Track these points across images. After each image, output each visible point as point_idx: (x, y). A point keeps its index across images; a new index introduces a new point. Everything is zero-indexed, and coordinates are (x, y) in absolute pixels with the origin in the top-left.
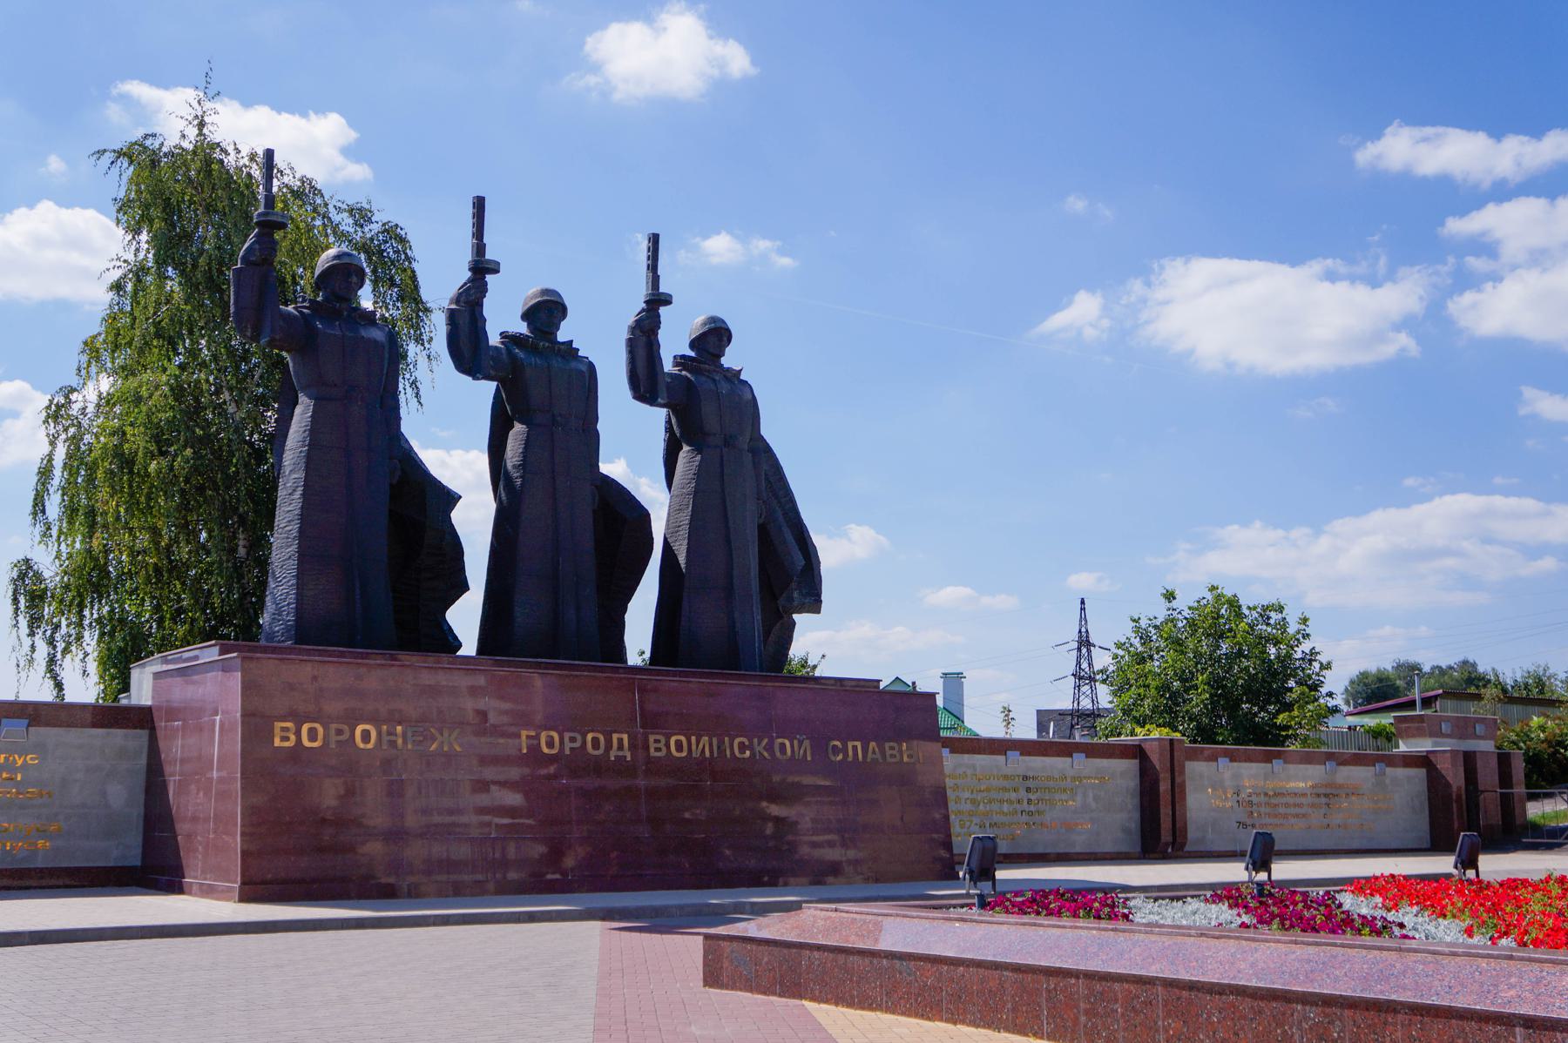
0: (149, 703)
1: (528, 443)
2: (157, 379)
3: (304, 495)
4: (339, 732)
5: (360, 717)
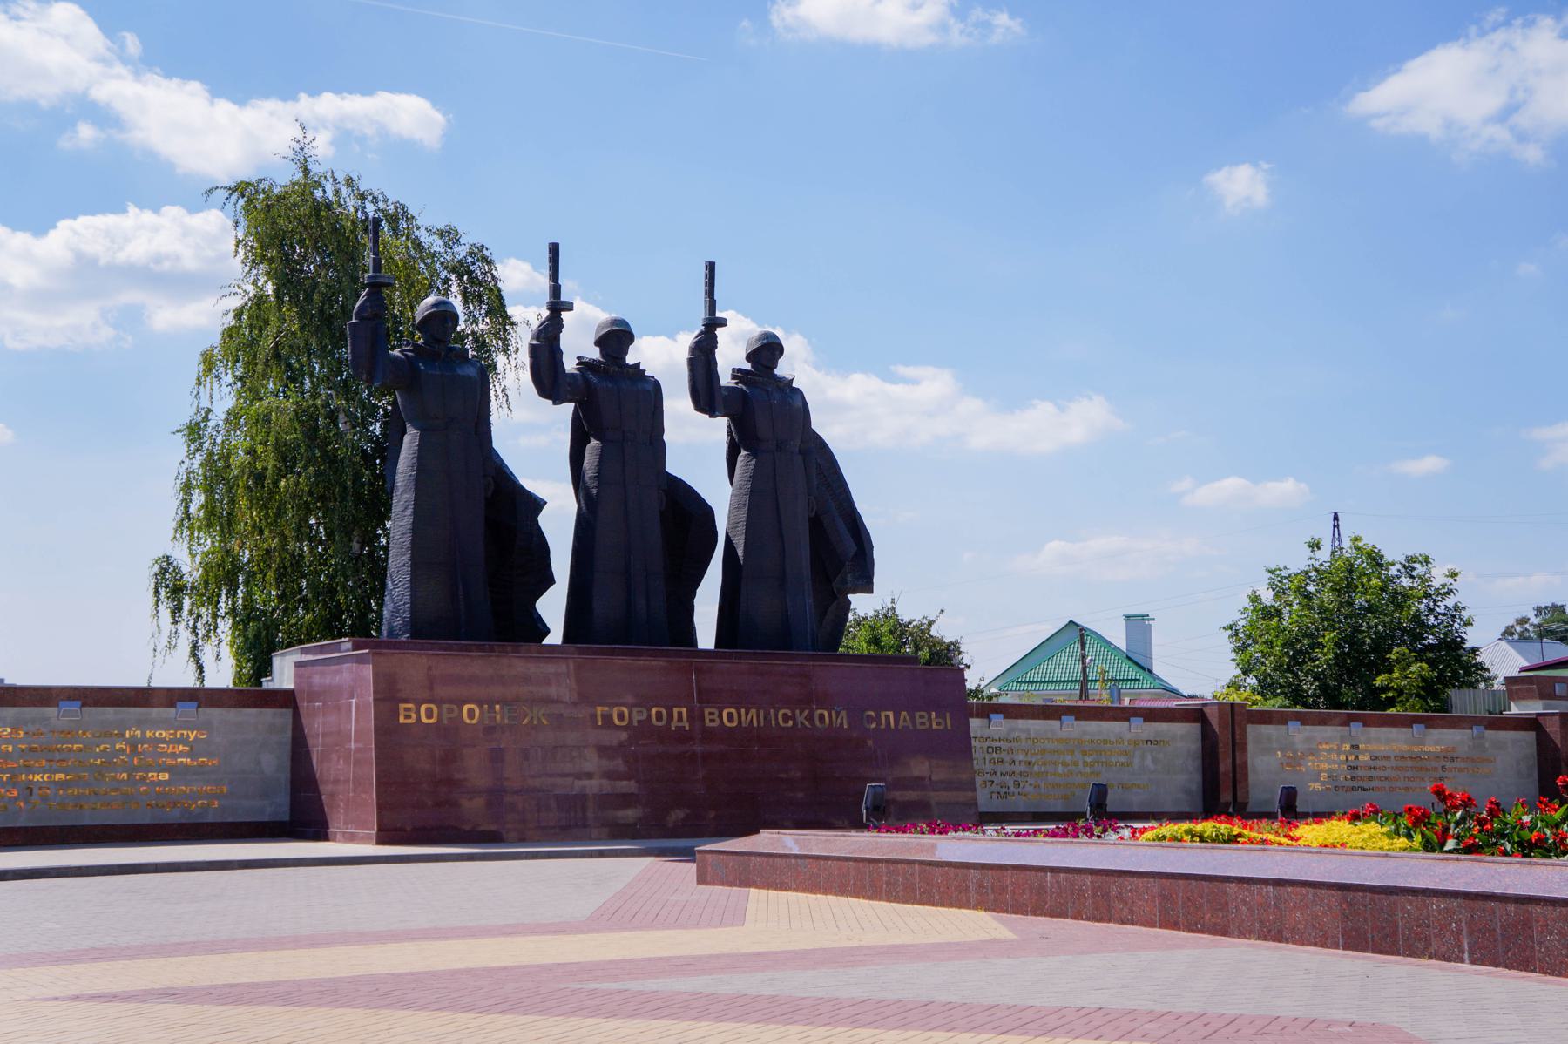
0: (291, 686)
1: (602, 458)
2: (280, 402)
3: (414, 512)
4: (450, 711)
5: (468, 697)
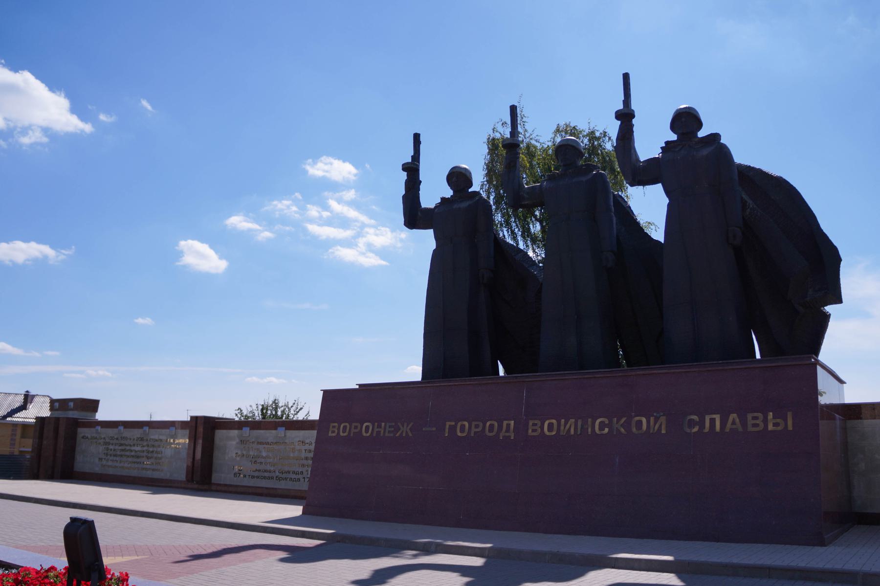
1: (149, 101)
